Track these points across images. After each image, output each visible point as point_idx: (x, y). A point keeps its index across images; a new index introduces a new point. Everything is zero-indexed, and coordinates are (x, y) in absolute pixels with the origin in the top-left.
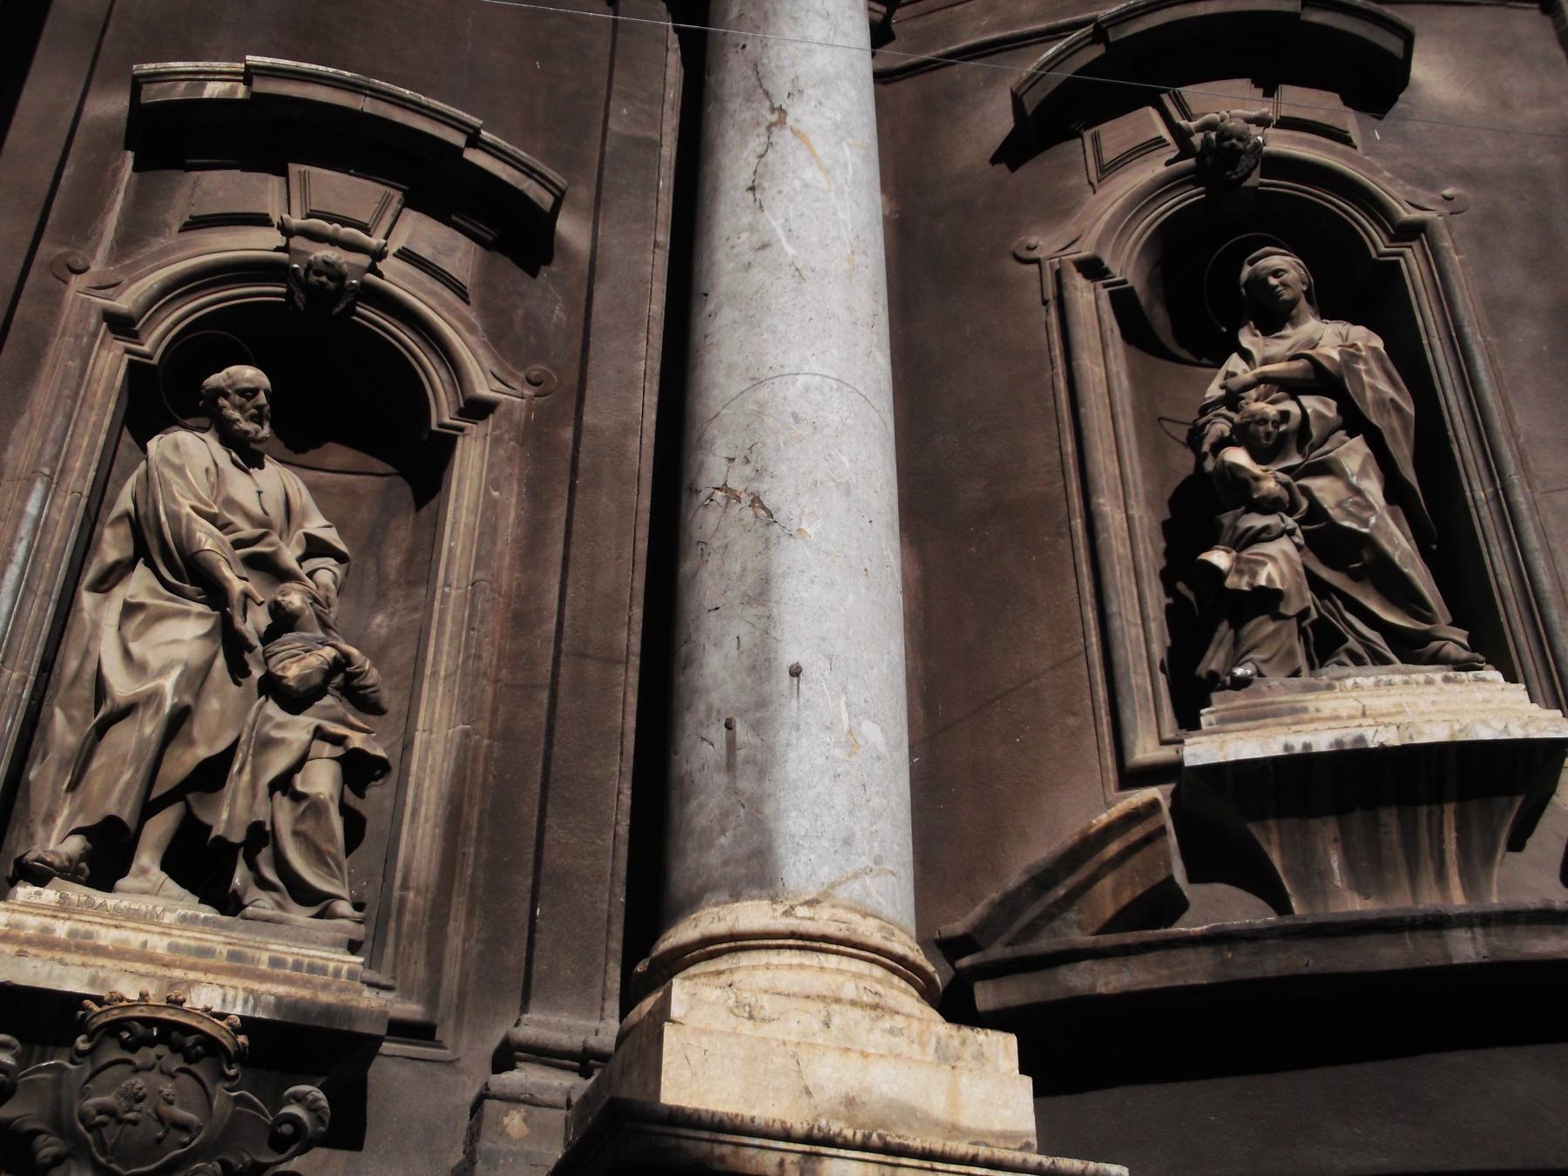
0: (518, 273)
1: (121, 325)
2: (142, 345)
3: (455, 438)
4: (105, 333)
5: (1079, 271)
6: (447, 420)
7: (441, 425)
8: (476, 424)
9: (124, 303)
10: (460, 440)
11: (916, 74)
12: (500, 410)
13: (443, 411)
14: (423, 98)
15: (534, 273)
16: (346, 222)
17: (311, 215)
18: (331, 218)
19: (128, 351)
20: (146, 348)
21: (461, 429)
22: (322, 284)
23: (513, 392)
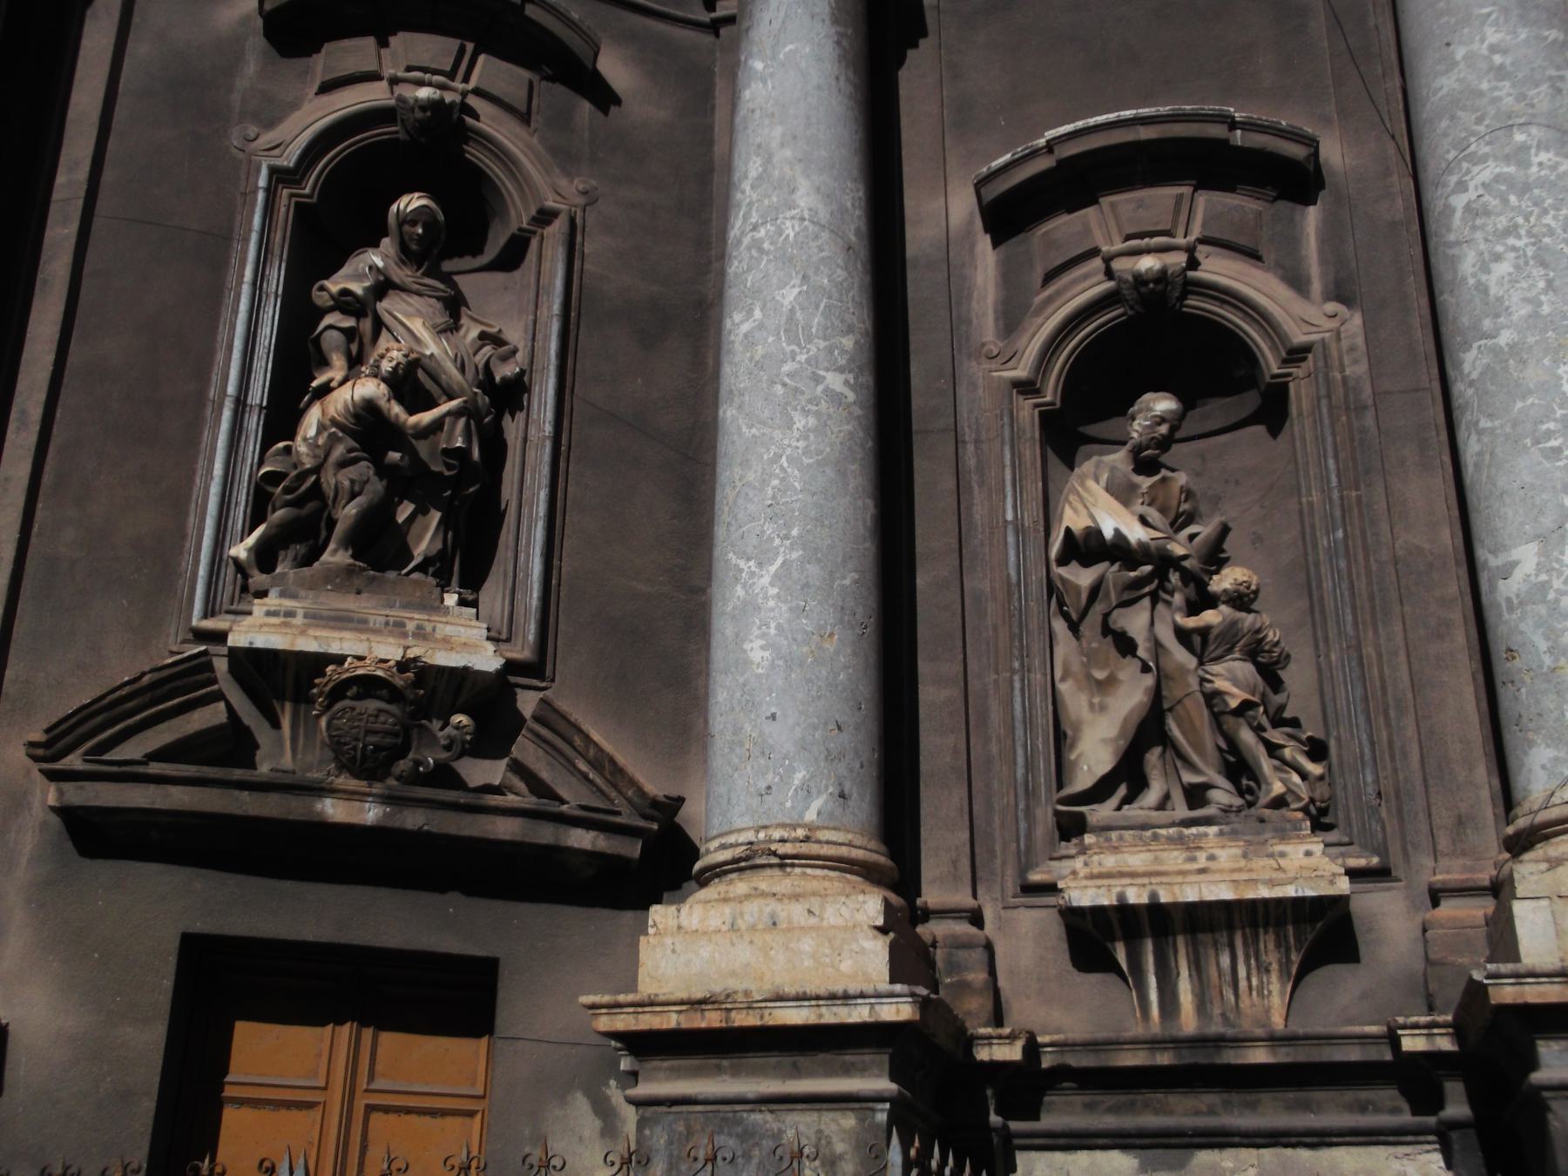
0: (199, 927)
1: (1026, 387)
2: (1045, 397)
3: (1285, 386)
4: (1202, 270)
5: (987, 230)
6: (1276, 371)
7: (1274, 376)
8: (1299, 367)
9: (1021, 372)
10: (1291, 385)
11: (1465, 896)
12: (1318, 349)
13: (1272, 364)
14: (1161, 109)
15: (190, 943)
16: (1152, 234)
17: (1128, 238)
18: (1141, 236)
19: (1037, 406)
20: (1048, 398)
21: (1289, 375)
22: (1153, 290)
23: (1315, 329)
